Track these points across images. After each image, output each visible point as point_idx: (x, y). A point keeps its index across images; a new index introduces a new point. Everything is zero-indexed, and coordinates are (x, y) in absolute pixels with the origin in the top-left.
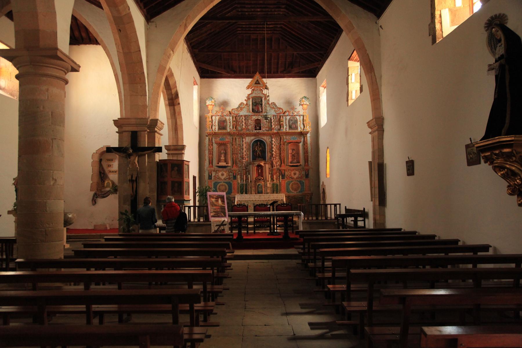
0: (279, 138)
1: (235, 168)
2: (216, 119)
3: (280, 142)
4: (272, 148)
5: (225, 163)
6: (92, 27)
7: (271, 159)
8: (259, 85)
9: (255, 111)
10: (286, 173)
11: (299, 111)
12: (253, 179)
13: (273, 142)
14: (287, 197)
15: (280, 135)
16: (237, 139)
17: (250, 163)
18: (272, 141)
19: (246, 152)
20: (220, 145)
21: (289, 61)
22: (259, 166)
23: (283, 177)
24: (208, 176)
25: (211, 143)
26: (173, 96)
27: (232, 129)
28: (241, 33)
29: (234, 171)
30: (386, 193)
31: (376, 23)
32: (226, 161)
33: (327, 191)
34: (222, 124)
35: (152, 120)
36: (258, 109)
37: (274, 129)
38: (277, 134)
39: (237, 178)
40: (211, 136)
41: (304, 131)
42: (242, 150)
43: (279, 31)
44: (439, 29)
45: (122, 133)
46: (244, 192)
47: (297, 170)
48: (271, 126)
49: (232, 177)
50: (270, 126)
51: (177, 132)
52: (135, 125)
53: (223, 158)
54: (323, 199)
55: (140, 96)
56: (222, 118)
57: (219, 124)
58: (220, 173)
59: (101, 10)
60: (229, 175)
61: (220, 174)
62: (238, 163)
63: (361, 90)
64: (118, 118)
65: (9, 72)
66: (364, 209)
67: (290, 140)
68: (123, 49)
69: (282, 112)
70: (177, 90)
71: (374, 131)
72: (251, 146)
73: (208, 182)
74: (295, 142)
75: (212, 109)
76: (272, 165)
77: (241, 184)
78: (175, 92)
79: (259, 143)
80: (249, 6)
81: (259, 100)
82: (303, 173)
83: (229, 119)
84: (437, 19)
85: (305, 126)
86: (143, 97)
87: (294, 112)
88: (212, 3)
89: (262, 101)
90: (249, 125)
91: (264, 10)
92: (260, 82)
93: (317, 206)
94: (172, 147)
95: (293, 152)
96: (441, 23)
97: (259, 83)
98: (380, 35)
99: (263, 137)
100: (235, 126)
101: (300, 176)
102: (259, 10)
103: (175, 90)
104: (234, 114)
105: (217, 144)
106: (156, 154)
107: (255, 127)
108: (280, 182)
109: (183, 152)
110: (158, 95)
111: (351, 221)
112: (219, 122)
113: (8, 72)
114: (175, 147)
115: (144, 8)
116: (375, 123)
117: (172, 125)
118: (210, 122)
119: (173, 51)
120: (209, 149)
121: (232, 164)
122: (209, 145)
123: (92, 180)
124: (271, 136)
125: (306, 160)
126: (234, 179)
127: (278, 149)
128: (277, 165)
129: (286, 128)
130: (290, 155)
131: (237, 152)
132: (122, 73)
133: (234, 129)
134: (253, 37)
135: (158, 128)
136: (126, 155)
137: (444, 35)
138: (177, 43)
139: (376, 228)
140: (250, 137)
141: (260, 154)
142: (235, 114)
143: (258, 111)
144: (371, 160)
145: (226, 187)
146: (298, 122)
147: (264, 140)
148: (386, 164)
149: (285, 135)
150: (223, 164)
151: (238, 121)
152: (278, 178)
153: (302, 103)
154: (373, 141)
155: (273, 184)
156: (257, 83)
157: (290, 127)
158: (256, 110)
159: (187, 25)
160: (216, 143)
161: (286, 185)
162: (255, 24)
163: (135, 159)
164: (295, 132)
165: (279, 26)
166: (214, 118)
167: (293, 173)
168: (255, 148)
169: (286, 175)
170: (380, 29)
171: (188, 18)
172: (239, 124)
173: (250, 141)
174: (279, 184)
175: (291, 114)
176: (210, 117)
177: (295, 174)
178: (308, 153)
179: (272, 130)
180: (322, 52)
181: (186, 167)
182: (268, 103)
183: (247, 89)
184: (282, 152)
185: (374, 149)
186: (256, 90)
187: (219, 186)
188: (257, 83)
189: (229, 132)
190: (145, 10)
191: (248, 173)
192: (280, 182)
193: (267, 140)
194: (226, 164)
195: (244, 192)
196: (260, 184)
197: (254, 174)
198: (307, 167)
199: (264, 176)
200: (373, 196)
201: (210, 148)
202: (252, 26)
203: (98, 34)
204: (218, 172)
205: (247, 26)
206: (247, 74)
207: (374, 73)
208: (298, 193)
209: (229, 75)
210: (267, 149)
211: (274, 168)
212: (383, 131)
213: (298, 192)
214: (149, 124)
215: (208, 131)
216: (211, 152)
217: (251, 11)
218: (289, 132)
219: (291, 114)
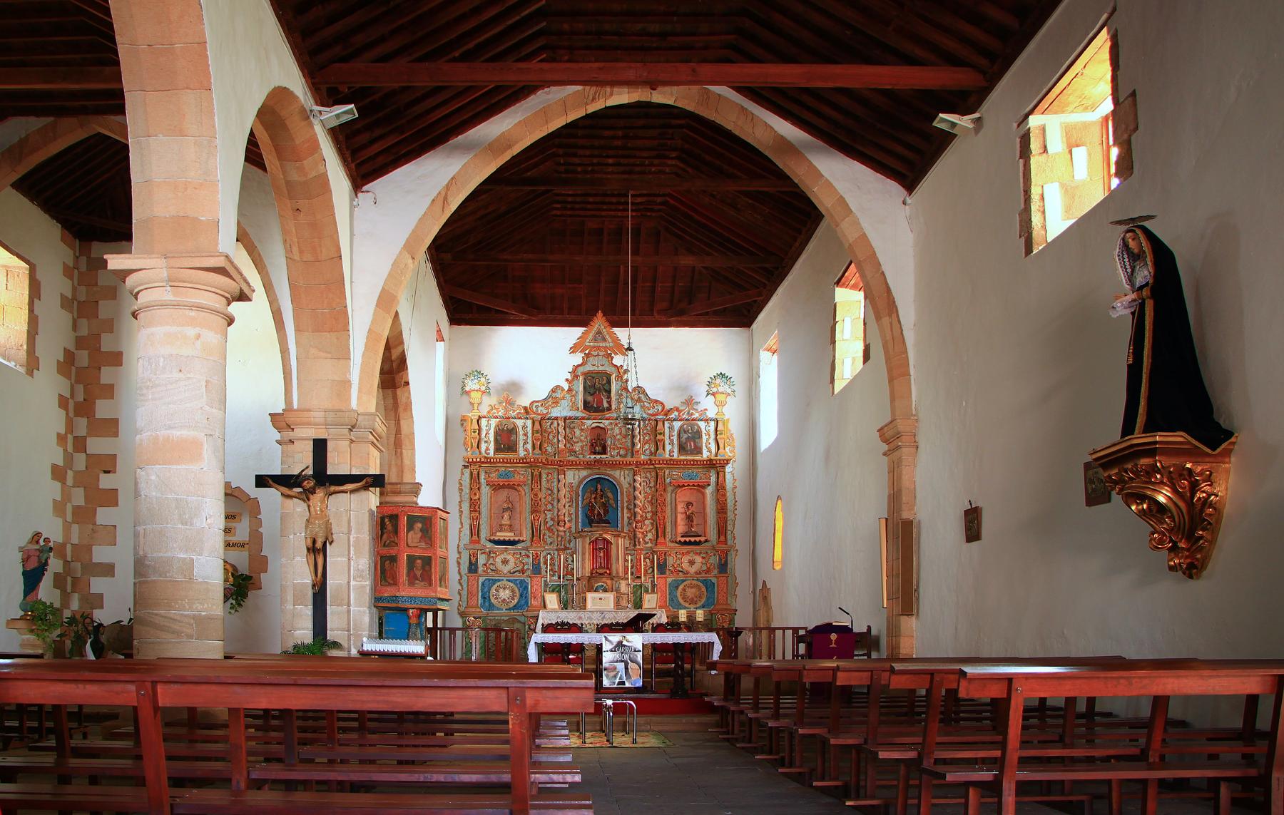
9: (592, 406)
11: (706, 410)
16: (544, 476)
18: (635, 481)
19: (567, 506)
34: (506, 439)
41: (719, 458)
42: (555, 504)
48: (633, 444)
56: (505, 422)
58: (499, 557)
59: (260, 171)
62: (544, 535)
66: (869, 627)
76: (634, 539)
80: (588, 152)
82: (714, 560)
83: (524, 427)
85: (721, 446)
89: (609, 382)
100: (539, 446)
101: (705, 568)
103: (399, 350)
108: (653, 582)
112: (496, 433)
115: (353, 162)
118: (474, 432)
120: (471, 499)
129: (672, 451)
130: (680, 517)
133: (537, 451)
146: (704, 435)
151: (546, 431)
153: (714, 390)
157: (682, 448)
166: (484, 422)
167: (686, 559)
175: (685, 416)
176: (475, 422)
177: (692, 563)
182: (626, 389)
186: (595, 356)
192: (653, 582)
193: (622, 478)
198: (723, 547)
206: (573, 317)
211: (638, 547)
213: (698, 606)
219: (684, 416)
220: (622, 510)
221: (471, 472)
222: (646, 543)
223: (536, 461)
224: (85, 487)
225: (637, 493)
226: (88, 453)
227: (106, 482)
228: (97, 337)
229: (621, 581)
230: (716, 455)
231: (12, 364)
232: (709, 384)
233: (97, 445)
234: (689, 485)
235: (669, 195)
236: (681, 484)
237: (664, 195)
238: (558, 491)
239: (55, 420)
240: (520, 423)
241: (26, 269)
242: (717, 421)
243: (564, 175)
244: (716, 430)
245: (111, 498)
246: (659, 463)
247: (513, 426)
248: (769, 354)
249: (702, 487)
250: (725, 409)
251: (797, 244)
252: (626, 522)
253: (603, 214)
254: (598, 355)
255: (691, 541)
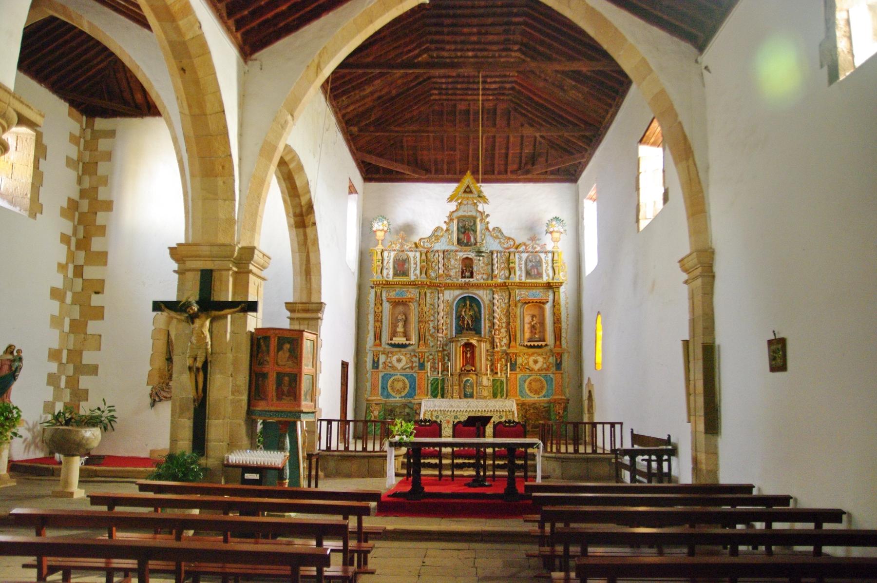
0: (507, 293)
1: (422, 349)
2: (390, 257)
3: (509, 301)
4: (494, 312)
5: (405, 339)
6: (142, 70)
7: (491, 332)
8: (470, 195)
9: (463, 242)
10: (520, 360)
11: (545, 244)
12: (456, 370)
13: (495, 301)
14: (522, 406)
15: (508, 288)
16: (428, 295)
17: (451, 340)
18: (493, 298)
19: (445, 317)
20: (396, 304)
21: (527, 151)
22: (468, 346)
23: (513, 367)
24: (372, 361)
25: (379, 301)
26: (304, 209)
27: (419, 275)
28: (440, 100)
29: (420, 354)
30: (720, 407)
31: (696, 61)
32: (406, 335)
33: (595, 396)
34: (401, 267)
35: (242, 248)
36: (469, 238)
37: (498, 276)
38: (503, 286)
39: (426, 368)
40: (380, 287)
41: (555, 281)
42: (436, 316)
43: (507, 95)
44: (845, 50)
45: (185, 273)
46: (439, 394)
47: (539, 355)
48: (493, 270)
49: (417, 365)
50: (490, 271)
51: (308, 276)
52: (209, 257)
53: (400, 329)
54: (588, 410)
55: (222, 201)
56: (400, 254)
57: (396, 266)
59: (146, 31)
60: (412, 362)
61: (394, 359)
62: (428, 340)
63: (666, 199)
64: (178, 244)
65: (9, 163)
66: (669, 436)
67: (527, 298)
68: (190, 106)
69: (514, 245)
70: (310, 199)
71: (696, 278)
72: (454, 309)
73: (372, 374)
74: (536, 302)
75: (383, 238)
76: (493, 344)
77: (433, 379)
78: (307, 201)
79: (468, 303)
80: (453, 47)
81: (471, 222)
82: (552, 360)
83: (415, 257)
84: (841, 28)
85: (557, 272)
86: (227, 202)
87: (535, 246)
88: (371, 26)
89: (475, 223)
90: (451, 269)
91: (479, 54)
92: (474, 190)
93: (577, 425)
94: (298, 305)
95: (533, 320)
96: (850, 38)
97: (471, 192)
98: (704, 86)
99: (477, 292)
100: (425, 270)
101: (545, 366)
102: (470, 54)
103: (307, 197)
104: (424, 247)
105: (390, 303)
106: (249, 317)
107: (463, 272)
108: (507, 376)
109: (320, 315)
110: (260, 200)
111: (643, 460)
112: (394, 262)
113: (7, 162)
114: (304, 305)
115: (237, 30)
116: (695, 261)
117: (301, 264)
118: (379, 261)
119: (292, 116)
120: (375, 312)
121: (417, 341)
122: (376, 304)
123: (151, 364)
124: (491, 290)
125: (558, 336)
126: (420, 370)
127: (504, 315)
128: (503, 343)
129: (520, 276)
130: (527, 326)
131: (427, 318)
132: (188, 156)
133: (424, 275)
134: (462, 106)
135: (256, 265)
136: (187, 317)
137: (859, 62)
138: (300, 101)
139: (699, 483)
140: (452, 291)
141: (470, 322)
142: (425, 248)
143: (467, 243)
144: (687, 338)
145: (404, 383)
146: (544, 264)
147: (480, 297)
148: (719, 346)
149: (518, 289)
150: (401, 340)
151: (430, 261)
152: (504, 368)
153: (551, 230)
154: (693, 298)
155: (493, 380)
156: (468, 191)
157: (528, 274)
158: (465, 241)
159: (322, 66)
160: (388, 301)
161: (518, 382)
162: (463, 83)
163: (202, 326)
164: (537, 283)
165: (508, 86)
166: (386, 254)
167: (531, 359)
168: (461, 311)
169: (518, 363)
170: (705, 72)
171: (323, 53)
172: (432, 266)
173: (451, 298)
174: (504, 380)
175: (530, 249)
176: (379, 253)
177: (536, 362)
178: (560, 323)
179: (494, 279)
180: (588, 134)
181: (309, 345)
182: (487, 229)
183: (449, 202)
184: (511, 320)
185: (693, 315)
186: (465, 205)
187: (393, 382)
188: (468, 191)
189: (413, 282)
190: (239, 35)
191: (447, 358)
192: (507, 376)
193: (485, 296)
194: (407, 340)
195: (439, 394)
196: (469, 380)
197: (457, 363)
198: (558, 350)
199: (478, 365)
200: (692, 412)
201: (377, 311)
202: (459, 86)
203: (151, 83)
204: (390, 355)
205: (450, 86)
206: (450, 176)
207: (694, 160)
208: (541, 399)
209: (416, 176)
210: (484, 313)
211: (496, 349)
212: (713, 277)
213: (540, 396)
214: (237, 256)
215: (375, 279)
216: (378, 319)
217: (456, 57)
218: (527, 283)
219: (529, 250)
220: (485, 320)
221: (376, 292)
222: (501, 346)
223: (422, 284)
224: (80, 305)
225: (495, 308)
226: (84, 278)
227: (96, 300)
228: (95, 189)
229: (483, 376)
230: (553, 279)
231: (17, 210)
232: (548, 226)
233: (91, 272)
234: (533, 302)
235: (516, 82)
236: (527, 301)
237: (511, 82)
238: (438, 306)
239: (60, 253)
240: (411, 255)
241: (33, 135)
242: (554, 253)
243: (436, 60)
244: (553, 260)
245: (99, 313)
246: (511, 285)
247: (406, 257)
248: (591, 202)
249: (540, 304)
250: (559, 244)
251: (609, 115)
252: (487, 330)
253: (469, 98)
254: (467, 204)
255: (536, 345)
